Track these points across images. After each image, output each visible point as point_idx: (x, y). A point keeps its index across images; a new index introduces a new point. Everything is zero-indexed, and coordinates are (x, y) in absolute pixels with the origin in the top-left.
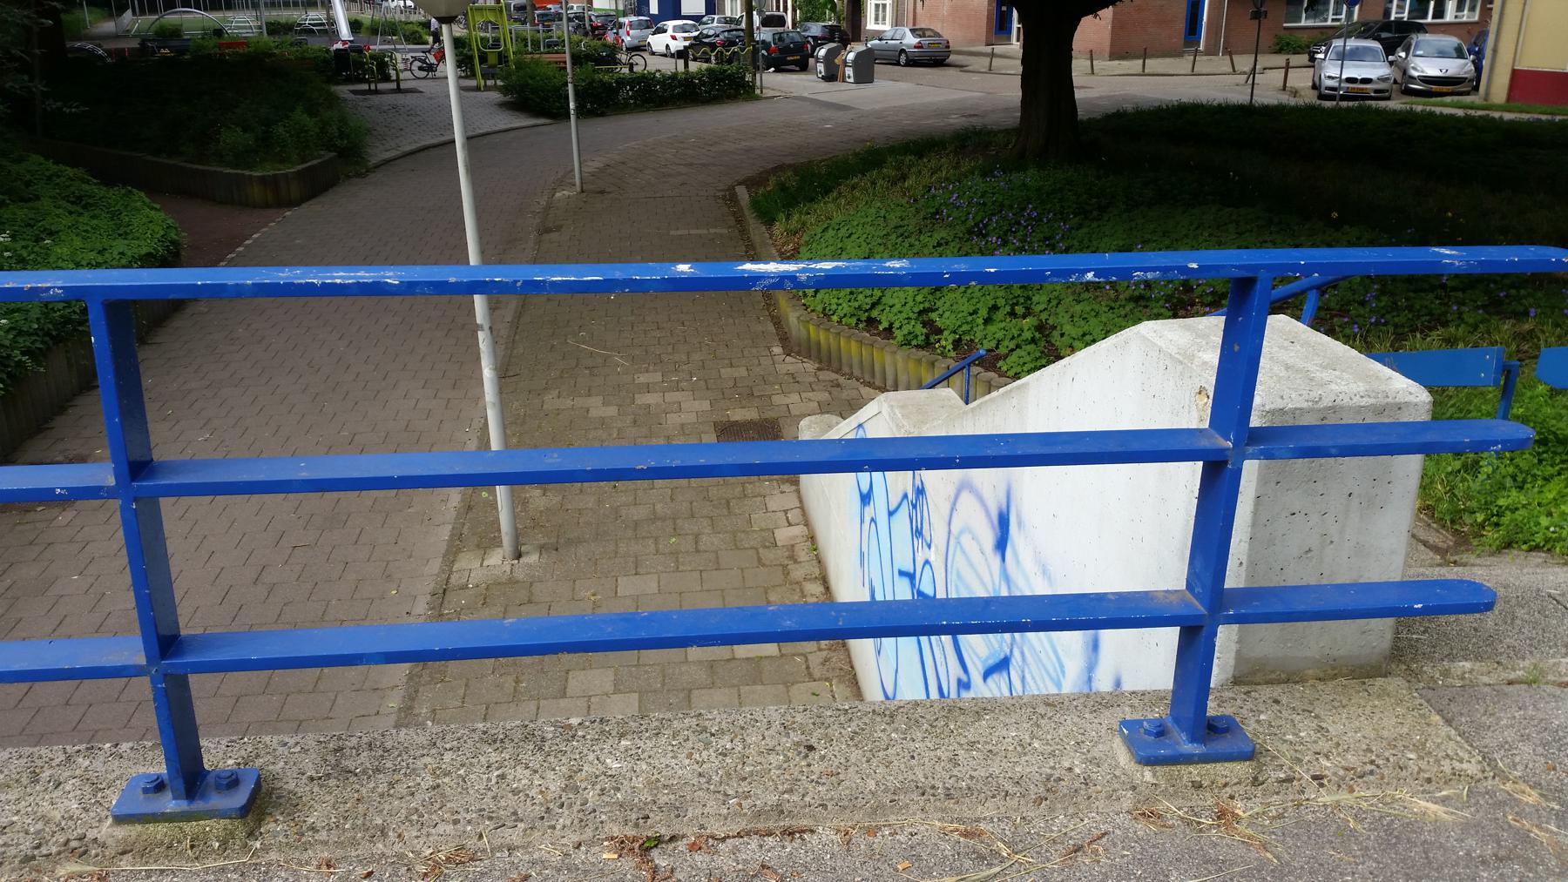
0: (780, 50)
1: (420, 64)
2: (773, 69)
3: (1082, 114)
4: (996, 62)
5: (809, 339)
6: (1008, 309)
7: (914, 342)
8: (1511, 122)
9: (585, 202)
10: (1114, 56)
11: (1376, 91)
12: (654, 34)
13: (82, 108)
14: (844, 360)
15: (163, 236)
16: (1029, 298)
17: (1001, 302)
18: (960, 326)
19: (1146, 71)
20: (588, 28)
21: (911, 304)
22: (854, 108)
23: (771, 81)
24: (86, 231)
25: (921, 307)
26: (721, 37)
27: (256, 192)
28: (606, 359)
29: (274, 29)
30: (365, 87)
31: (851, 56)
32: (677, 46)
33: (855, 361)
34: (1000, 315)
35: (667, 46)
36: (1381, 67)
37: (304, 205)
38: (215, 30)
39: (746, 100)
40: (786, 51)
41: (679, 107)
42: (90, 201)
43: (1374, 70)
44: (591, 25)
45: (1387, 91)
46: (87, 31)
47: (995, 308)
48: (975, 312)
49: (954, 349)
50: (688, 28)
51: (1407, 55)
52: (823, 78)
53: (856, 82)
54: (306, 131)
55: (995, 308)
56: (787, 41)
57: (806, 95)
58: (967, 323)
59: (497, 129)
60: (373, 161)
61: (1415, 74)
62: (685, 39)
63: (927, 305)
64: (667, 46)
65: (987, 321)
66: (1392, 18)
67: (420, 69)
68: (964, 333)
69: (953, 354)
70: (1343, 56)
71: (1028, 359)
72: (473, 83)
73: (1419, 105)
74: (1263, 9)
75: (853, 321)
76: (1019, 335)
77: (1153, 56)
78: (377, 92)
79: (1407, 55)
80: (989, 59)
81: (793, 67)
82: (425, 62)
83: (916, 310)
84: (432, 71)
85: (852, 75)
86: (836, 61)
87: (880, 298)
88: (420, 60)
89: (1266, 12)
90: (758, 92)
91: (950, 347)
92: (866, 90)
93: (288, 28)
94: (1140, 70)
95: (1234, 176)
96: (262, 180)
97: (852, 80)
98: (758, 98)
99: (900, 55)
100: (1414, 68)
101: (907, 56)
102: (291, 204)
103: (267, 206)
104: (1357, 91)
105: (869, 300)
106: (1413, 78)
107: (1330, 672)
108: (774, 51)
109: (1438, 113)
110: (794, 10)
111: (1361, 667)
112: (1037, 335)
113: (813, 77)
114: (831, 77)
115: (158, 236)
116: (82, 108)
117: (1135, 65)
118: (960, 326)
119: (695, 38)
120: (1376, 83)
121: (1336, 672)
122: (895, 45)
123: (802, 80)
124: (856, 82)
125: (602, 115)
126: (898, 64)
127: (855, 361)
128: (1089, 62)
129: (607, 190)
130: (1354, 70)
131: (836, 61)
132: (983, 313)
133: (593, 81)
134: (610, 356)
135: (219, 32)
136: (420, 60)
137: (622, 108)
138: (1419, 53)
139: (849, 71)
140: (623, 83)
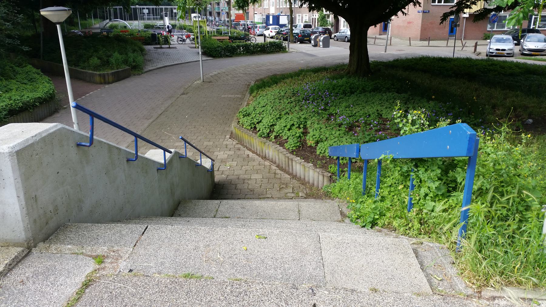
0: (302, 36)
1: (180, 39)
2: (299, 42)
3: (371, 60)
4: (377, 41)
5: (236, 133)
6: (297, 125)
7: (263, 136)
8: (530, 65)
9: (202, 85)
10: (421, 39)
11: (507, 54)
12: (266, 30)
13: (30, 49)
14: (244, 141)
15: (47, 92)
16: (306, 122)
17: (295, 123)
18: (279, 131)
19: (430, 45)
20: (247, 28)
21: (269, 122)
22: (317, 56)
23: (298, 46)
24: (23, 89)
25: (272, 124)
26: (285, 31)
27: (97, 79)
28: (170, 137)
29: (147, 27)
30: (159, 46)
31: (322, 38)
32: (273, 34)
33: (247, 141)
34: (294, 128)
35: (269, 34)
36: (511, 45)
37: (113, 84)
38: (124, 26)
39: (282, 53)
40: (304, 36)
41: (259, 55)
42: (34, 80)
43: (508, 46)
44: (248, 27)
45: (512, 54)
46: (93, 26)
47: (293, 125)
48: (286, 126)
49: (275, 138)
50: (276, 28)
51: (524, 41)
52: (313, 45)
53: (323, 47)
54: (118, 60)
55: (293, 125)
56: (305, 32)
57: (304, 51)
58: (282, 130)
59: (193, 61)
60: (146, 70)
61: (525, 48)
62: (275, 32)
63: (274, 123)
64: (269, 34)
65: (289, 130)
66: (531, 28)
67: (181, 41)
68: (281, 133)
69: (274, 140)
70: (499, 41)
71: (293, 143)
72: (194, 46)
73: (530, 61)
74: (458, 23)
75: (249, 128)
76: (295, 135)
77: (431, 40)
78: (162, 48)
79: (524, 41)
80: (374, 40)
81: (307, 42)
82: (182, 39)
83: (270, 125)
84: (184, 41)
85: (322, 45)
86: (317, 40)
87: (261, 120)
88: (180, 38)
89: (459, 24)
90: (287, 50)
91: (273, 138)
92: (326, 49)
93: (152, 27)
94: (446, 46)
95: (408, 83)
96: (100, 75)
97: (322, 46)
98: (287, 52)
99: (345, 38)
100: (525, 46)
101: (348, 39)
102: (109, 83)
103: (101, 83)
104: (500, 53)
105: (257, 121)
106: (524, 49)
107: (6, 244)
108: (300, 36)
109: (515, 62)
110: (318, 23)
111: (17, 243)
112: (302, 135)
113: (310, 45)
114: (316, 45)
115: (45, 92)
116: (30, 49)
117: (426, 43)
118: (279, 131)
119: (277, 32)
120: (507, 51)
121: (8, 244)
122: (344, 35)
123: (308, 46)
124: (323, 47)
125: (231, 57)
126: (345, 41)
127: (247, 141)
128: (409, 41)
129: (213, 81)
130: (501, 46)
131: (317, 40)
132: (288, 127)
133: (228, 45)
134: (172, 136)
135: (125, 27)
136: (180, 38)
137: (239, 55)
138: (528, 40)
139: (321, 43)
140: (239, 46)
